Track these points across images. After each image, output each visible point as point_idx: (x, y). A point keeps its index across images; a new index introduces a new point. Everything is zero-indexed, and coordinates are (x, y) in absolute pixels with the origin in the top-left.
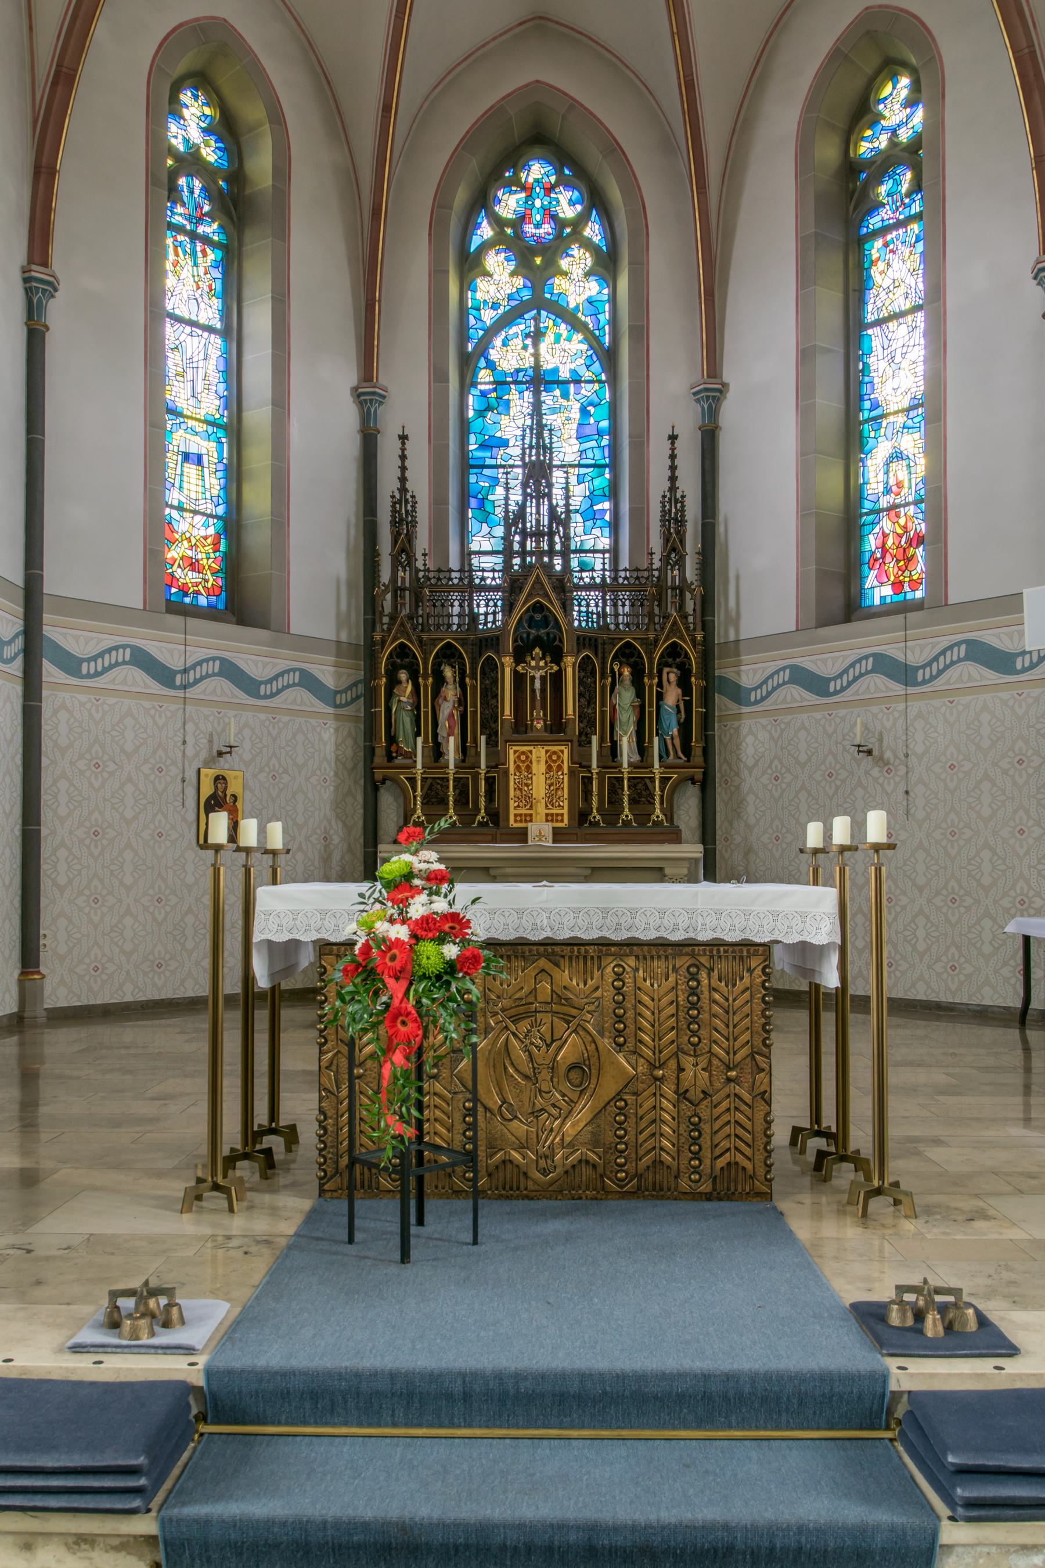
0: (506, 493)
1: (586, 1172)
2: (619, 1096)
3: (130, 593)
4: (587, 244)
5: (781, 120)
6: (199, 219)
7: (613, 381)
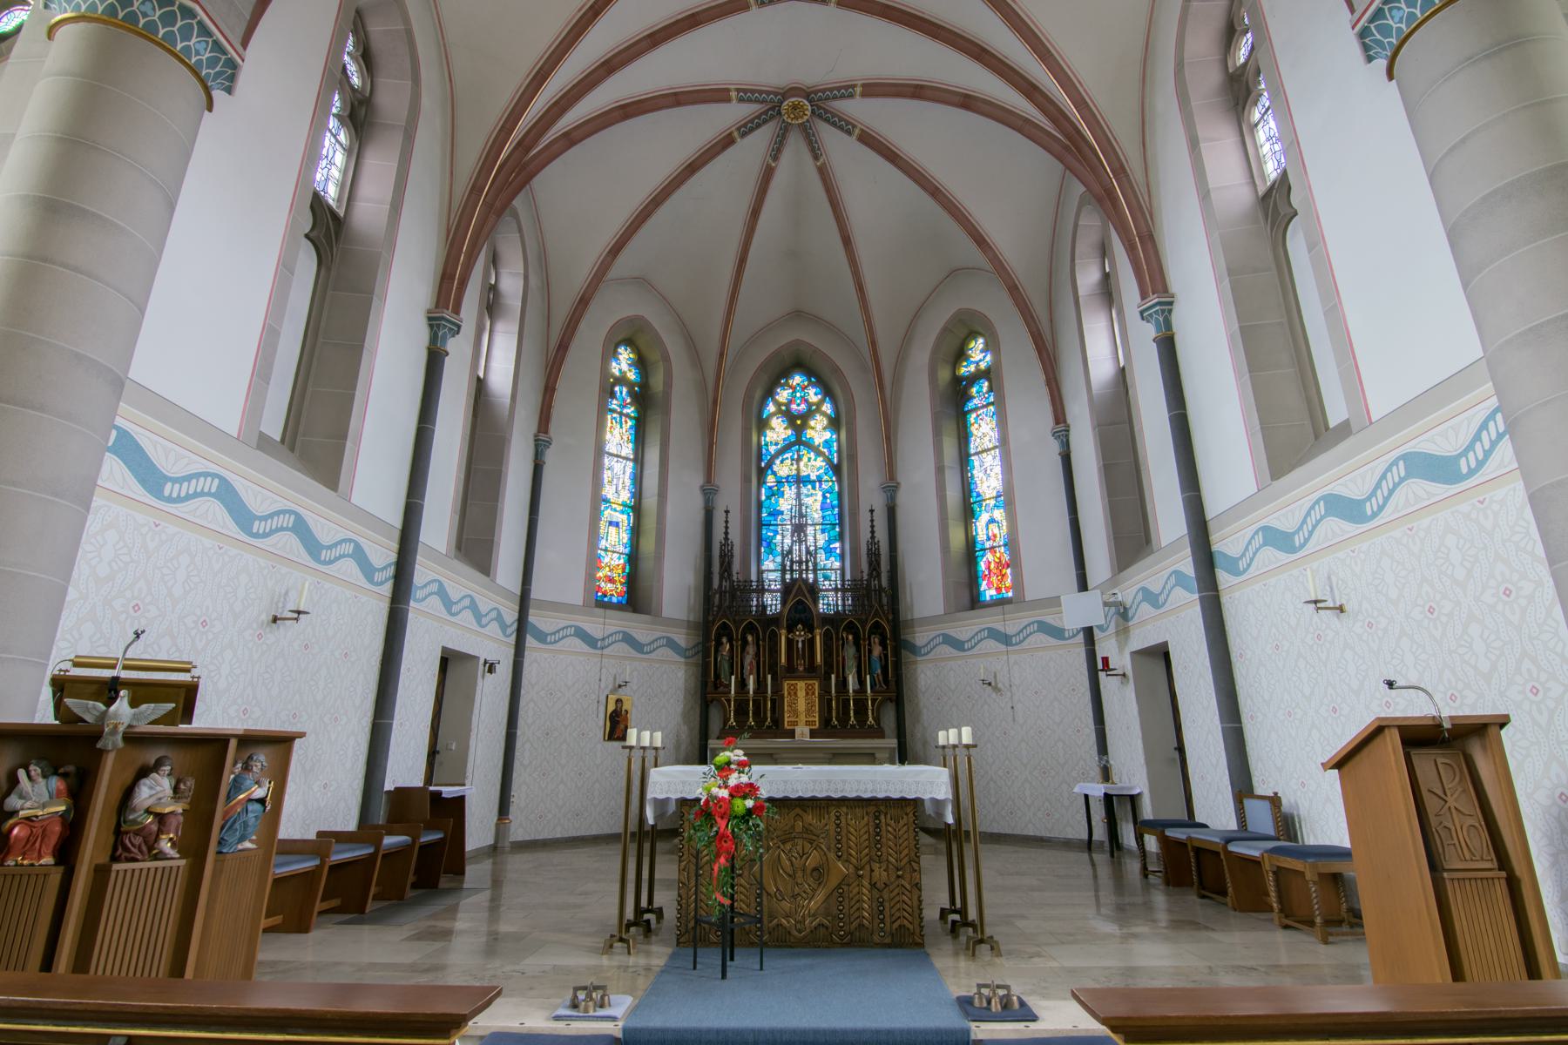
0: (783, 539)
1: (822, 930)
2: (839, 886)
3: (576, 596)
4: (824, 414)
5: (920, 357)
6: (625, 406)
7: (839, 481)
